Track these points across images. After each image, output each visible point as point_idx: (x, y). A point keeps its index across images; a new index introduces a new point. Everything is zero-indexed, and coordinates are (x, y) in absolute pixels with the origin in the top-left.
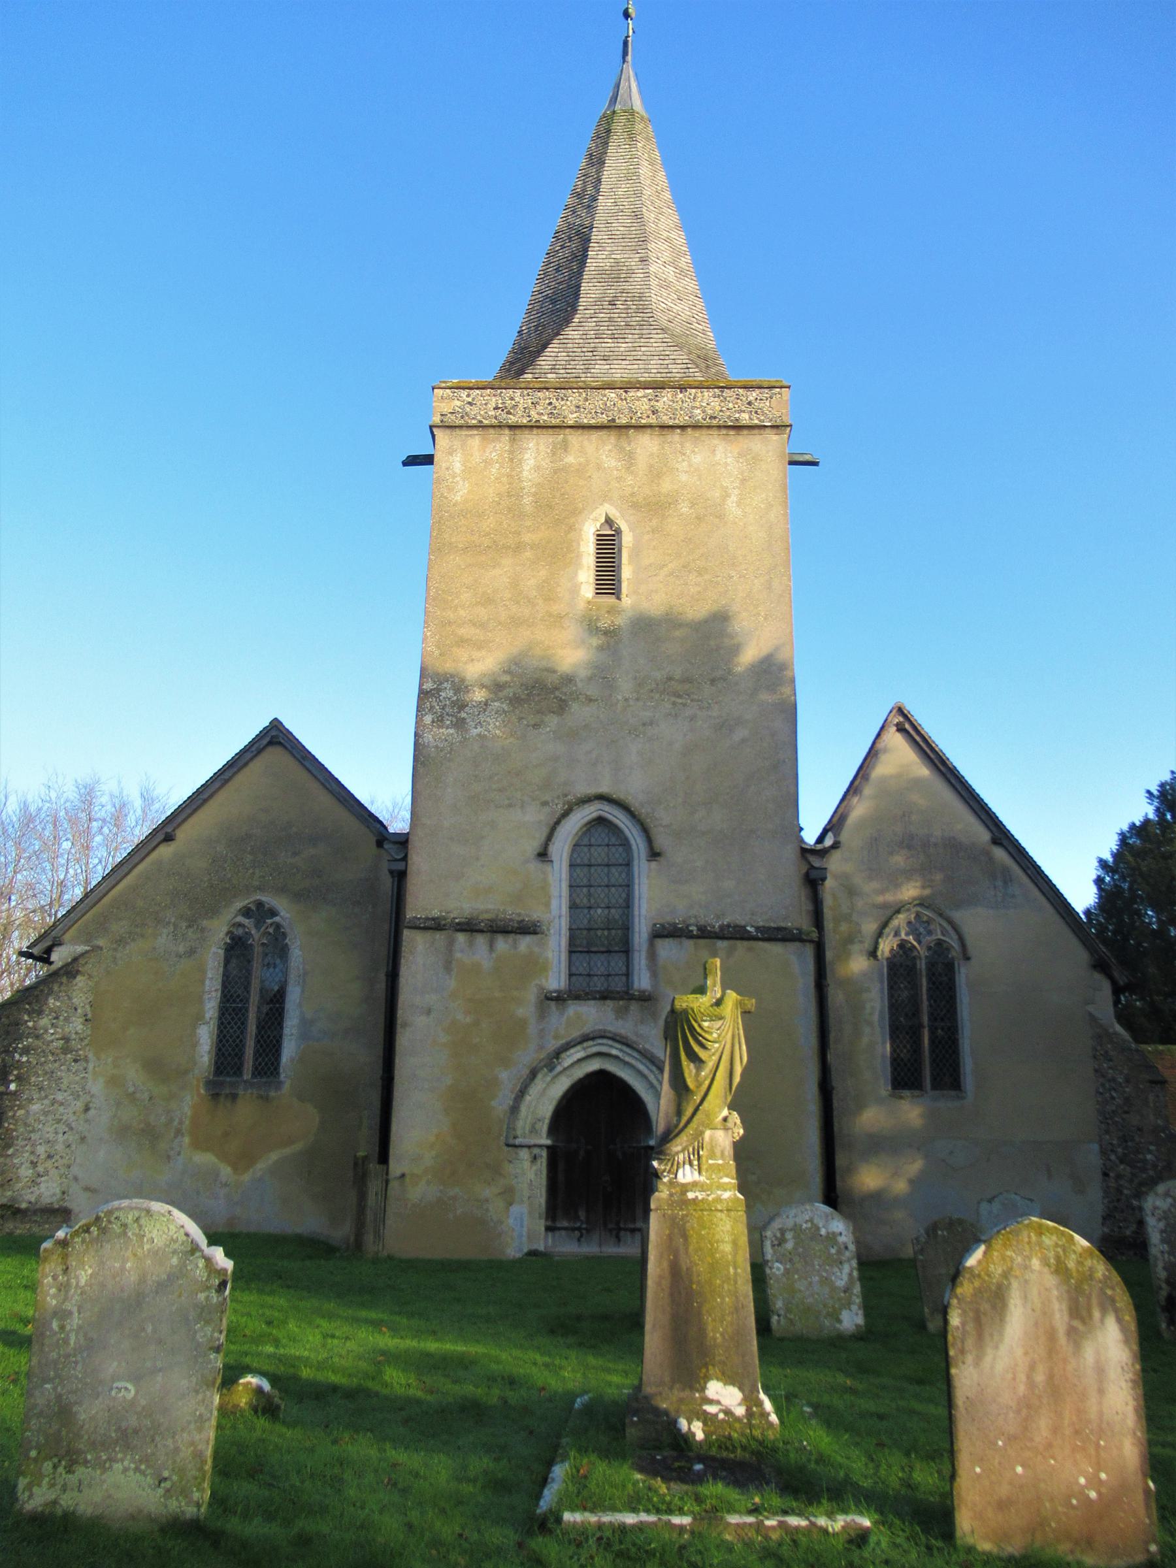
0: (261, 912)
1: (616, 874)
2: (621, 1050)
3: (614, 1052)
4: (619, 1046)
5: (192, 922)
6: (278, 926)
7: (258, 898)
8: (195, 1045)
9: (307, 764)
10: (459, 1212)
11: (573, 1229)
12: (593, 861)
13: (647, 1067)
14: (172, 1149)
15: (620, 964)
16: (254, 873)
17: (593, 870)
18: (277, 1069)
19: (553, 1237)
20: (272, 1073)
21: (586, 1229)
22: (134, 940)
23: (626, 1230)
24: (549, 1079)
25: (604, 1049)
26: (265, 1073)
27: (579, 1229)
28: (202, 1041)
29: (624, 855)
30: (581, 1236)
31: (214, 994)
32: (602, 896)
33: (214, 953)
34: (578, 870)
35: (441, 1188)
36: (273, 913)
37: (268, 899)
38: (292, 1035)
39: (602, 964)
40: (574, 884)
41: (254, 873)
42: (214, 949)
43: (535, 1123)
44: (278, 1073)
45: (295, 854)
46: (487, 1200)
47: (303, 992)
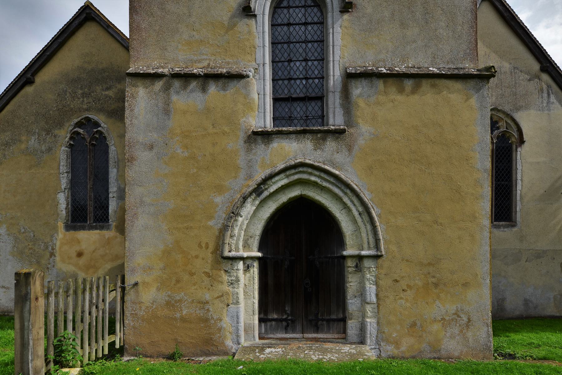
0: (87, 123)
1: (312, 49)
2: (319, 177)
3: (313, 178)
4: (317, 173)
5: (48, 132)
6: (101, 133)
7: (87, 115)
8: (58, 203)
9: (110, 30)
10: (184, 312)
11: (281, 320)
12: (292, 21)
13: (343, 191)
14: (49, 264)
15: (316, 108)
16: (83, 101)
17: (291, 29)
18: (107, 217)
19: (266, 326)
20: (105, 220)
21: (291, 320)
22: (14, 143)
23: (323, 320)
24: (257, 202)
25: (305, 176)
26: (101, 220)
27: (286, 320)
28: (60, 202)
29: (319, 14)
30: (288, 325)
31: (66, 175)
32: (301, 68)
33: (64, 150)
34: (279, 29)
35: (170, 293)
36: (97, 125)
37: (93, 116)
38: (113, 197)
39: (301, 109)
40: (276, 41)
41: (83, 101)
42: (63, 148)
43: (248, 239)
44: (109, 220)
45: (108, 89)
46: (207, 302)
47: (118, 171)
